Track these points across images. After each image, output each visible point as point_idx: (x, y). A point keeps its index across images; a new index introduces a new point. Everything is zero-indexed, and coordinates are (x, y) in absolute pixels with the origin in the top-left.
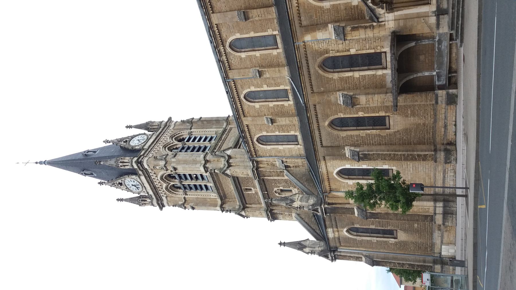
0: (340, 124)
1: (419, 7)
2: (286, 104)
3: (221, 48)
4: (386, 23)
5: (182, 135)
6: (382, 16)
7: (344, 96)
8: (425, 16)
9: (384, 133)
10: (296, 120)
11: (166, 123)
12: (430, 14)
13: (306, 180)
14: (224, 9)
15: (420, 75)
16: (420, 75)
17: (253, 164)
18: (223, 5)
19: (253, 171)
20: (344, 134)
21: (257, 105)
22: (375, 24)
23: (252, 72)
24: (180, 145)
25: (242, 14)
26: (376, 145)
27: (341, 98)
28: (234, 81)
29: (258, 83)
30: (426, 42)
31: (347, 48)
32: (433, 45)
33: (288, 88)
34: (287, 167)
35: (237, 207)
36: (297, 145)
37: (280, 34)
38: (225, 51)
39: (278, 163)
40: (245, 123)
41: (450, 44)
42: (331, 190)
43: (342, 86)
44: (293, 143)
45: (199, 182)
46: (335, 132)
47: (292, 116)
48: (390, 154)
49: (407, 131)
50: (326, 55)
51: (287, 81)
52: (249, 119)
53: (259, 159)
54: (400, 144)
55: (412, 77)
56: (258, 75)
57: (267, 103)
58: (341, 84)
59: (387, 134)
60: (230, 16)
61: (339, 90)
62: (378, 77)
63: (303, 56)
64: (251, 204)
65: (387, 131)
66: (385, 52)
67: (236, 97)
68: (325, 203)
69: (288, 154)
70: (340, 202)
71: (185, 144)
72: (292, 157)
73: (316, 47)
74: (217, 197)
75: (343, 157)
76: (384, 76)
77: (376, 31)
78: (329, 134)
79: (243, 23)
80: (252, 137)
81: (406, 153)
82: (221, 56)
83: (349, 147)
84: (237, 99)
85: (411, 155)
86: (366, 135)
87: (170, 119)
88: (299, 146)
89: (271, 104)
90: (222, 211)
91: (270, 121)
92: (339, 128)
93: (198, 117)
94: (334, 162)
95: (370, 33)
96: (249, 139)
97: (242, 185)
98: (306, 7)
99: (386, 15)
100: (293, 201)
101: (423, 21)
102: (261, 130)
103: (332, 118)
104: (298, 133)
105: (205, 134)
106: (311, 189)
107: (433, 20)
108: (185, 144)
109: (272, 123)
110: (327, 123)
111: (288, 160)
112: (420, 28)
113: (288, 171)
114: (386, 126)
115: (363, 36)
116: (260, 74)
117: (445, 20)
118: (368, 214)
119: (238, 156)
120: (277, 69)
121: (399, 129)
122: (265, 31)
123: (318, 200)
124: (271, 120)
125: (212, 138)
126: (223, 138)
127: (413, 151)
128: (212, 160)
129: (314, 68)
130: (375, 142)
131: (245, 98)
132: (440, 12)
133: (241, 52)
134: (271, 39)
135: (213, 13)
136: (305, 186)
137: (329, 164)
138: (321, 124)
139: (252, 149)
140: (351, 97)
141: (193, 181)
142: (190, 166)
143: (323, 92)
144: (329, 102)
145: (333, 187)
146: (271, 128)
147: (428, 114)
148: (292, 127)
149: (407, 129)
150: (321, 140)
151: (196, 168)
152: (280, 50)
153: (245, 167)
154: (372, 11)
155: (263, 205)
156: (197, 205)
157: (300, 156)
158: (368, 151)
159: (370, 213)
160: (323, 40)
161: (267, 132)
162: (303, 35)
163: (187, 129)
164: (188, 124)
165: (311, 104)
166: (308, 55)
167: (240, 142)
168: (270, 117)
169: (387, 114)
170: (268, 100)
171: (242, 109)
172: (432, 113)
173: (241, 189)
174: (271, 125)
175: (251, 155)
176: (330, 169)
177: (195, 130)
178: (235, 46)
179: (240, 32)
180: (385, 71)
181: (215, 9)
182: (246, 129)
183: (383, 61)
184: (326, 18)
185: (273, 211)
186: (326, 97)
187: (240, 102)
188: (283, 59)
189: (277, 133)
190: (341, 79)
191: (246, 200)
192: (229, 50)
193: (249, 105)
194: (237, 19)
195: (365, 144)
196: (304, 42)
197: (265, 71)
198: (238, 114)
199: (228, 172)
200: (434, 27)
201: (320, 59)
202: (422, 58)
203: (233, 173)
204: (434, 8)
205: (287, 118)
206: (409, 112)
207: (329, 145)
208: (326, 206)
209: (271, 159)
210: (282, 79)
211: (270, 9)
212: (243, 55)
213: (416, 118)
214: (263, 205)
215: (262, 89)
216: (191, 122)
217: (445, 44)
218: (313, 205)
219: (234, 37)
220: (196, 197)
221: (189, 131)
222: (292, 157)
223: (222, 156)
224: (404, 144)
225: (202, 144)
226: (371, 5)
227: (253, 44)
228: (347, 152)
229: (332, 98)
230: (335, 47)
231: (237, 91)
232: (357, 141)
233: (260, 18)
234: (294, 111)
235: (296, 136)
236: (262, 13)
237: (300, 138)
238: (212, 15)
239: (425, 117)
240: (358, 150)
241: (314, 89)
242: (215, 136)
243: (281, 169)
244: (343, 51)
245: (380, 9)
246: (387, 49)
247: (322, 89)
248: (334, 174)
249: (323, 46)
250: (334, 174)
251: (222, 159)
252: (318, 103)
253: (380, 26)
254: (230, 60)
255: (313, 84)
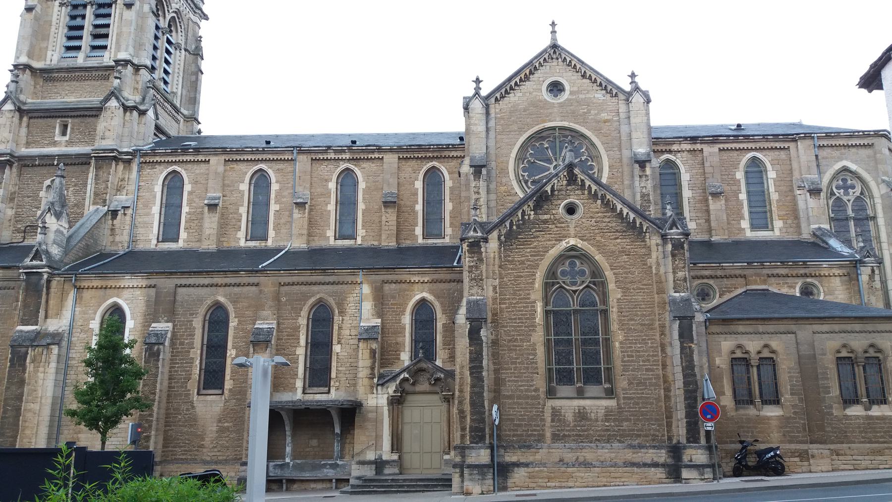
0: (217, 320)
1: (390, 438)
2: (241, 234)
3: (347, 156)
4: (375, 396)
5: (177, 32)
6: (385, 389)
7: (270, 331)
8: (378, 446)
9: (193, 386)
10: (209, 245)
11: (200, 9)
12: (378, 452)
13: (87, 245)
14: (402, 175)
15: (289, 439)
16: (289, 439)
17: (127, 153)
18: (407, 175)
19: (112, 150)
20: (197, 324)
21: (244, 187)
22: (375, 380)
23: (304, 194)
24: (163, 24)
25: (393, 200)
26: (170, 372)
27: (267, 326)
28: (292, 160)
29: (284, 197)
30: (337, 447)
31: (343, 341)
32: (331, 458)
33: (270, 243)
34: (114, 213)
35: (22, 97)
36: (158, 239)
37: (356, 246)
38: (342, 160)
39: (122, 199)
40: (214, 160)
41: (331, 480)
42: (79, 288)
43: (285, 328)
44: (161, 233)
45: (86, 41)
46: (202, 310)
47: (219, 241)
48: (154, 394)
49: (193, 420)
50: (337, 312)
51: (282, 244)
52: (221, 169)
53: (135, 167)
54: (167, 409)
55: (287, 428)
56: (299, 201)
57: (246, 204)
58: (288, 328)
59: (189, 390)
60: (391, 180)
61: (278, 324)
62: (292, 381)
63: (341, 279)
64: (28, 126)
65: (196, 391)
66: (329, 392)
67: (264, 157)
68: (51, 276)
69: (139, 219)
70: (51, 302)
71: (163, 34)
72: (133, 226)
73: (352, 299)
74: (48, 62)
75: (151, 315)
76: (293, 389)
77: (366, 382)
78: (201, 301)
79: (378, 198)
80: (184, 165)
81: (154, 419)
82: (336, 152)
83: (171, 329)
84: (260, 157)
85: (150, 426)
86: (192, 359)
87: (206, 18)
88: (154, 242)
89: (243, 210)
90: (15, 66)
91: (212, 202)
92: (207, 318)
93: (203, 69)
94: (142, 302)
95: (363, 373)
96: (181, 158)
97: (76, 120)
98: (407, 293)
99: (386, 396)
100: (58, 216)
101: (371, 443)
102: (195, 183)
103: (231, 308)
104: (181, 244)
105: (174, 72)
106: (73, 251)
107: (371, 456)
108: (163, 34)
109: (209, 205)
110: (222, 299)
111: (128, 218)
112: (361, 438)
113: (105, 214)
114: (204, 389)
115: (361, 364)
116: (301, 205)
117: (369, 472)
118: (23, 350)
119: (142, 129)
120: (305, 232)
121: (197, 409)
122: (363, 226)
123: (56, 262)
124: (216, 205)
125: (166, 83)
126: (166, 104)
127: (157, 430)
128: (138, 78)
129: (321, 293)
130: (177, 371)
131: (261, 170)
132: (379, 465)
133: (337, 183)
134: (350, 232)
135: (399, 158)
136: (79, 242)
137: (138, 292)
138: (221, 289)
139: (158, 159)
140: (267, 342)
141: (91, 28)
142: (132, 36)
143: (279, 301)
144: (258, 307)
145: (87, 294)
146: (197, 200)
147: (219, 451)
148: (197, 234)
149: (195, 420)
150: (189, 286)
151: (127, 46)
152: (332, 242)
153: (120, 137)
154: (394, 378)
155: (23, 150)
156: (37, 19)
157: (133, 240)
158: (163, 359)
159: (27, 353)
160: (360, 310)
161: (190, 193)
162: (371, 283)
163: (186, 43)
164: (193, 47)
165: (262, 279)
166: (341, 286)
167: (160, 136)
168: (220, 205)
169: (226, 392)
170: (251, 206)
171: (240, 160)
172: (220, 458)
173: (68, 117)
174: (206, 202)
175: (146, 155)
176: (126, 293)
177: (183, 57)
178: (347, 179)
179: (366, 191)
180: (300, 391)
181: (404, 162)
182: (200, 158)
183: (315, 390)
184: (389, 317)
185: (8, 167)
186: (270, 303)
187: (255, 160)
188: (318, 243)
189: (185, 209)
190: (297, 329)
191: (40, 120)
192: (343, 166)
193: (246, 173)
194: (386, 190)
195: (174, 355)
196: (361, 283)
197: (304, 213)
198: (231, 152)
199: (113, 103)
200: (361, 458)
201: (332, 302)
202: (314, 442)
203: (109, 112)
204: (385, 457)
205: (215, 232)
206: (226, 424)
207: (179, 298)
208: (45, 276)
209: (132, 187)
210: (286, 235)
211: (395, 239)
212: (332, 185)
213: (215, 435)
214: (24, 151)
215: (272, 202)
216: (197, 53)
217: (330, 473)
218: (47, 252)
219: (360, 179)
220: (54, 23)
221: (183, 46)
222: (133, 226)
223: (144, 99)
224: (168, 415)
225: (160, 65)
226: (402, 376)
227: (347, 204)
228: (163, 326)
229: (266, 313)
230: (346, 325)
231: (273, 160)
232: (182, 344)
233: (383, 223)
234: (225, 244)
235: (176, 240)
236: (391, 228)
237: (172, 246)
238: (396, 156)
239: (215, 447)
240: (167, 344)
241: (286, 288)
242: (169, 90)
243: (111, 202)
244: (339, 335)
245: (394, 388)
246: (334, 395)
247: (284, 299)
248: (115, 299)
249: (351, 309)
250: (115, 299)
251: (138, 98)
252: (261, 291)
253: (372, 387)
254: (326, 163)
255: (295, 287)
